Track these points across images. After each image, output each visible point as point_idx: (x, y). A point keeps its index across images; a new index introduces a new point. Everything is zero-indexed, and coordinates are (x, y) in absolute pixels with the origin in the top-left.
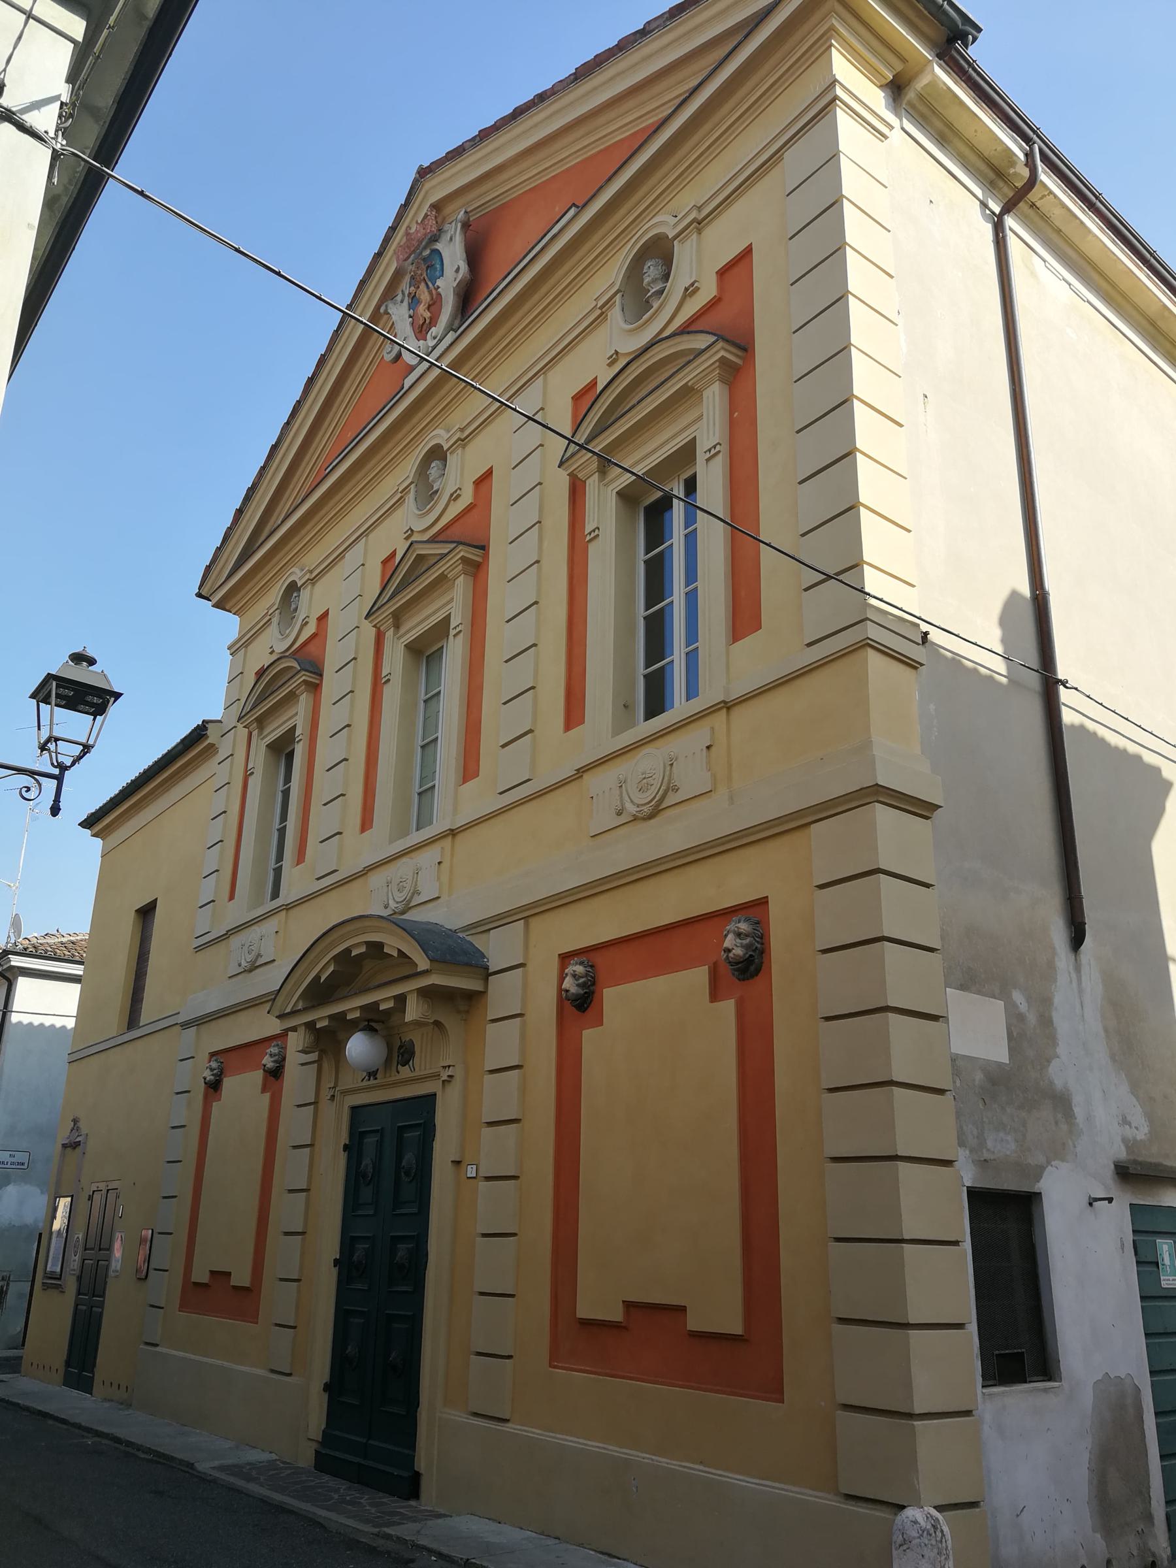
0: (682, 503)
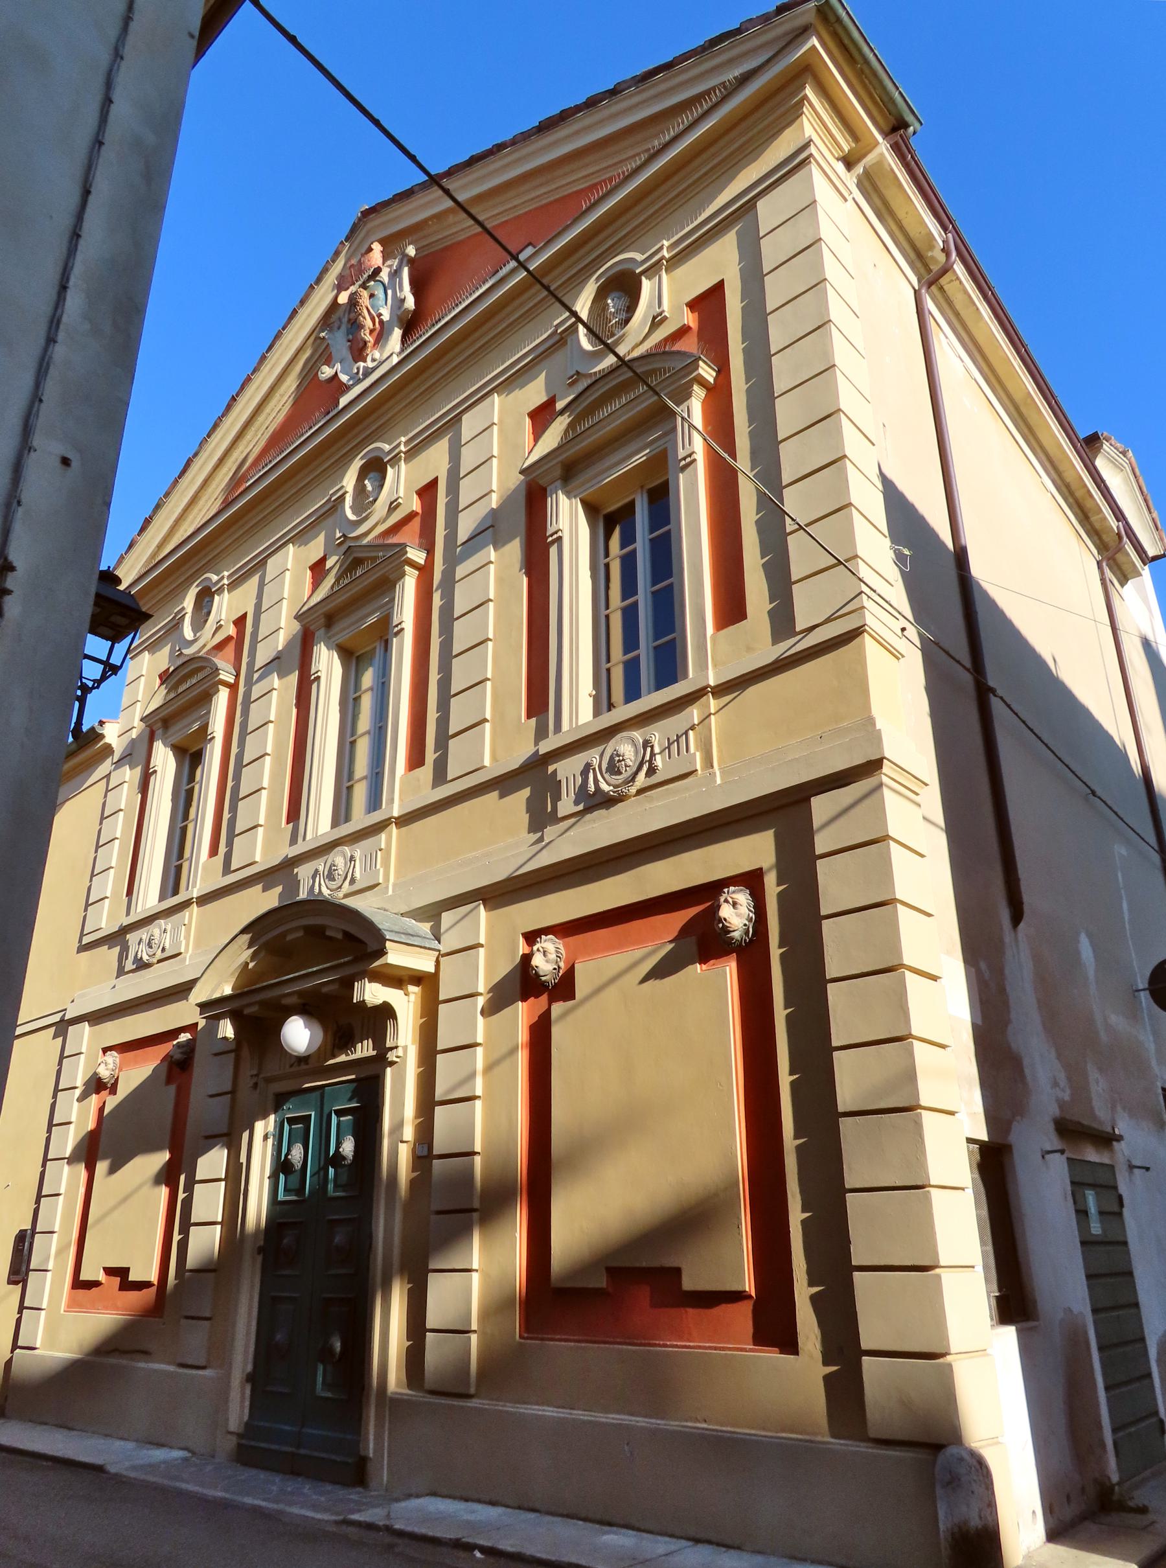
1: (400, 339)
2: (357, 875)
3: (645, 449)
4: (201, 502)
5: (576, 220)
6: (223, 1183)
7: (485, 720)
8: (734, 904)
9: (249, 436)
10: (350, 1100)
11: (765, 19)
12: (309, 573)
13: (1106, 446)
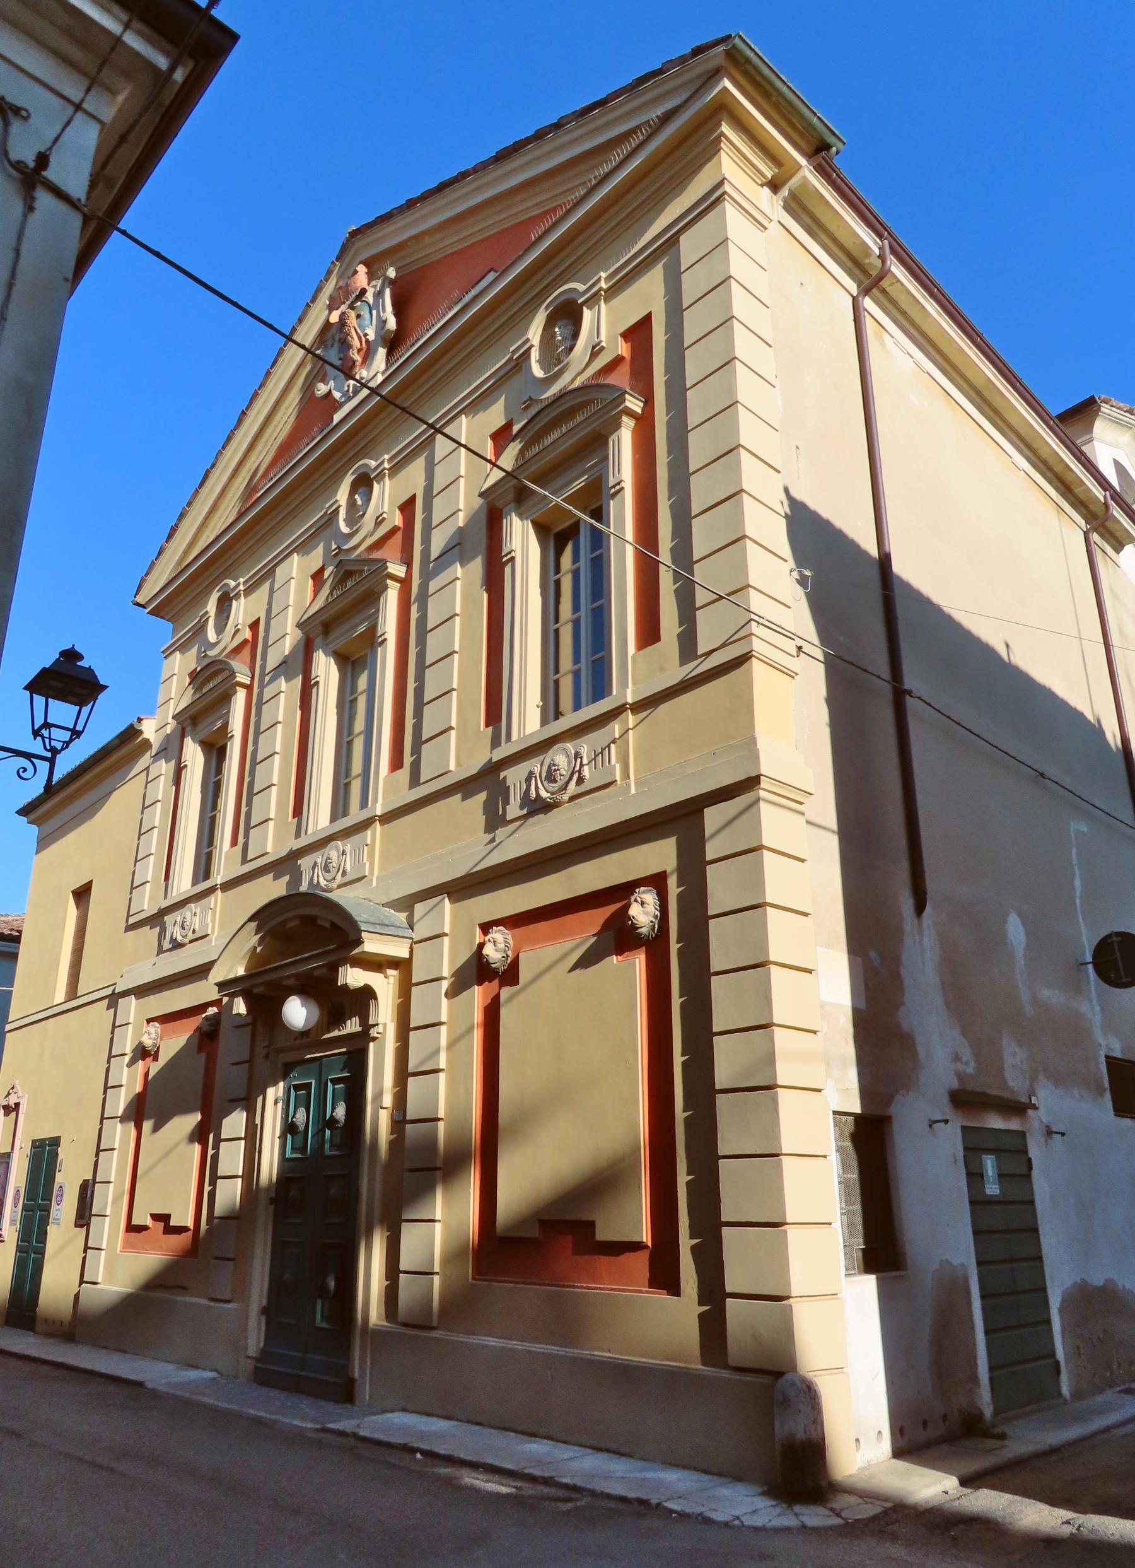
0: (627, 539)
1: (385, 357)
2: (348, 868)
3: (583, 476)
4: (221, 510)
5: (527, 251)
6: (243, 1142)
7: (451, 728)
8: (643, 903)
9: (260, 446)
10: (342, 1070)
11: (683, 60)
12: (310, 581)
13: (1105, 408)
